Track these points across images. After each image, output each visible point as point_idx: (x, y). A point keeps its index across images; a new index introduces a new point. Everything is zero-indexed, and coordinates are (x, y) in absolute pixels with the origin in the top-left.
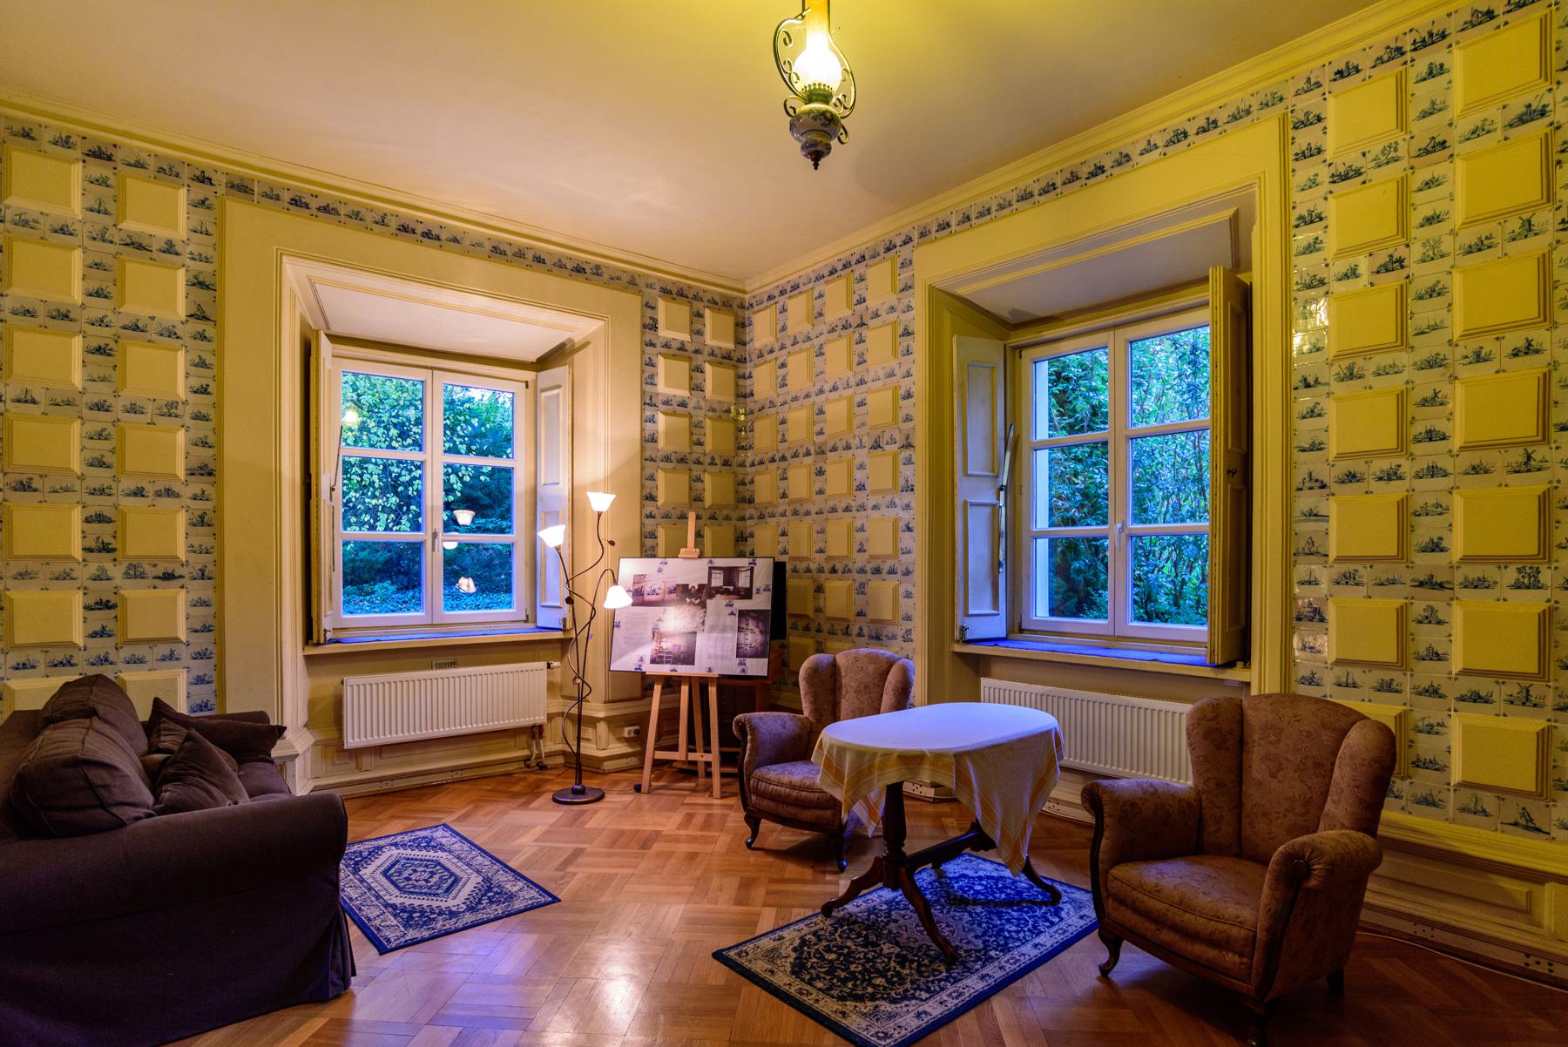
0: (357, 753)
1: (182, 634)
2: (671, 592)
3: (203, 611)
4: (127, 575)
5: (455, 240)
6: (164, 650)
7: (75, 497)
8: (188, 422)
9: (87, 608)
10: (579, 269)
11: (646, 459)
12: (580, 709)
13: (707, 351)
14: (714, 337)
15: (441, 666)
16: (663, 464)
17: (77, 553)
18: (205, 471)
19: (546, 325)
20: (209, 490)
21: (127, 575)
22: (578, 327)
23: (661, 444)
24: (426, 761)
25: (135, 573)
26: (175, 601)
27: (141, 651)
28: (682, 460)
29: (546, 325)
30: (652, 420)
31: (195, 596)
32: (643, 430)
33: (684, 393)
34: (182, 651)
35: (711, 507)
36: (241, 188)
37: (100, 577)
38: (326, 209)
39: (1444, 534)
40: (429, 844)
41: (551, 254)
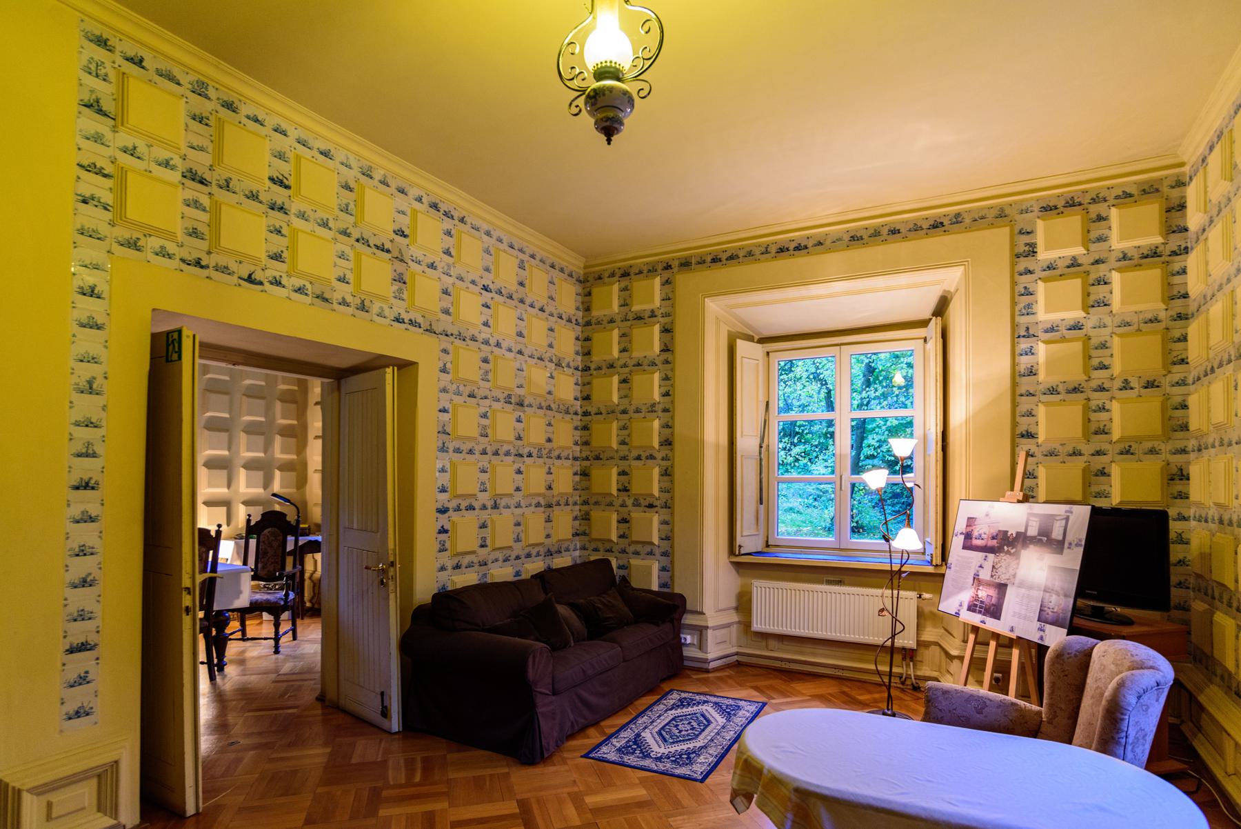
0: (765, 636)
1: (656, 541)
2: (993, 538)
3: (665, 527)
4: (634, 505)
5: (820, 244)
6: (648, 549)
7: (614, 462)
8: (660, 414)
9: (619, 522)
10: (937, 225)
11: (1016, 394)
12: (893, 643)
13: (1113, 257)
14: (1122, 238)
15: (829, 582)
16: (1043, 398)
17: (615, 492)
18: (667, 443)
19: (910, 286)
20: (670, 454)
21: (634, 505)
22: (949, 278)
23: (1041, 376)
24: (814, 655)
25: (637, 504)
26: (651, 520)
27: (638, 548)
28: (1075, 390)
29: (910, 286)
30: (1030, 352)
31: (662, 518)
32: (1014, 364)
33: (1077, 314)
34: (657, 551)
35: (1120, 440)
36: (685, 264)
37: (623, 505)
38: (731, 258)
39: (1108, 295)
40: (690, 703)
41: (906, 222)
